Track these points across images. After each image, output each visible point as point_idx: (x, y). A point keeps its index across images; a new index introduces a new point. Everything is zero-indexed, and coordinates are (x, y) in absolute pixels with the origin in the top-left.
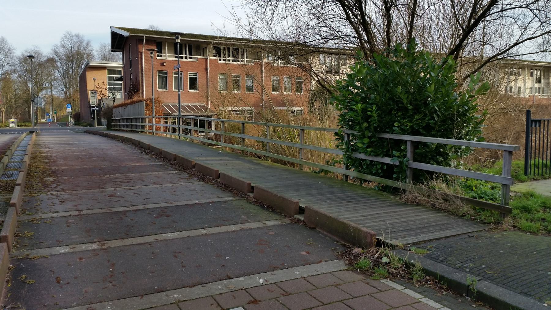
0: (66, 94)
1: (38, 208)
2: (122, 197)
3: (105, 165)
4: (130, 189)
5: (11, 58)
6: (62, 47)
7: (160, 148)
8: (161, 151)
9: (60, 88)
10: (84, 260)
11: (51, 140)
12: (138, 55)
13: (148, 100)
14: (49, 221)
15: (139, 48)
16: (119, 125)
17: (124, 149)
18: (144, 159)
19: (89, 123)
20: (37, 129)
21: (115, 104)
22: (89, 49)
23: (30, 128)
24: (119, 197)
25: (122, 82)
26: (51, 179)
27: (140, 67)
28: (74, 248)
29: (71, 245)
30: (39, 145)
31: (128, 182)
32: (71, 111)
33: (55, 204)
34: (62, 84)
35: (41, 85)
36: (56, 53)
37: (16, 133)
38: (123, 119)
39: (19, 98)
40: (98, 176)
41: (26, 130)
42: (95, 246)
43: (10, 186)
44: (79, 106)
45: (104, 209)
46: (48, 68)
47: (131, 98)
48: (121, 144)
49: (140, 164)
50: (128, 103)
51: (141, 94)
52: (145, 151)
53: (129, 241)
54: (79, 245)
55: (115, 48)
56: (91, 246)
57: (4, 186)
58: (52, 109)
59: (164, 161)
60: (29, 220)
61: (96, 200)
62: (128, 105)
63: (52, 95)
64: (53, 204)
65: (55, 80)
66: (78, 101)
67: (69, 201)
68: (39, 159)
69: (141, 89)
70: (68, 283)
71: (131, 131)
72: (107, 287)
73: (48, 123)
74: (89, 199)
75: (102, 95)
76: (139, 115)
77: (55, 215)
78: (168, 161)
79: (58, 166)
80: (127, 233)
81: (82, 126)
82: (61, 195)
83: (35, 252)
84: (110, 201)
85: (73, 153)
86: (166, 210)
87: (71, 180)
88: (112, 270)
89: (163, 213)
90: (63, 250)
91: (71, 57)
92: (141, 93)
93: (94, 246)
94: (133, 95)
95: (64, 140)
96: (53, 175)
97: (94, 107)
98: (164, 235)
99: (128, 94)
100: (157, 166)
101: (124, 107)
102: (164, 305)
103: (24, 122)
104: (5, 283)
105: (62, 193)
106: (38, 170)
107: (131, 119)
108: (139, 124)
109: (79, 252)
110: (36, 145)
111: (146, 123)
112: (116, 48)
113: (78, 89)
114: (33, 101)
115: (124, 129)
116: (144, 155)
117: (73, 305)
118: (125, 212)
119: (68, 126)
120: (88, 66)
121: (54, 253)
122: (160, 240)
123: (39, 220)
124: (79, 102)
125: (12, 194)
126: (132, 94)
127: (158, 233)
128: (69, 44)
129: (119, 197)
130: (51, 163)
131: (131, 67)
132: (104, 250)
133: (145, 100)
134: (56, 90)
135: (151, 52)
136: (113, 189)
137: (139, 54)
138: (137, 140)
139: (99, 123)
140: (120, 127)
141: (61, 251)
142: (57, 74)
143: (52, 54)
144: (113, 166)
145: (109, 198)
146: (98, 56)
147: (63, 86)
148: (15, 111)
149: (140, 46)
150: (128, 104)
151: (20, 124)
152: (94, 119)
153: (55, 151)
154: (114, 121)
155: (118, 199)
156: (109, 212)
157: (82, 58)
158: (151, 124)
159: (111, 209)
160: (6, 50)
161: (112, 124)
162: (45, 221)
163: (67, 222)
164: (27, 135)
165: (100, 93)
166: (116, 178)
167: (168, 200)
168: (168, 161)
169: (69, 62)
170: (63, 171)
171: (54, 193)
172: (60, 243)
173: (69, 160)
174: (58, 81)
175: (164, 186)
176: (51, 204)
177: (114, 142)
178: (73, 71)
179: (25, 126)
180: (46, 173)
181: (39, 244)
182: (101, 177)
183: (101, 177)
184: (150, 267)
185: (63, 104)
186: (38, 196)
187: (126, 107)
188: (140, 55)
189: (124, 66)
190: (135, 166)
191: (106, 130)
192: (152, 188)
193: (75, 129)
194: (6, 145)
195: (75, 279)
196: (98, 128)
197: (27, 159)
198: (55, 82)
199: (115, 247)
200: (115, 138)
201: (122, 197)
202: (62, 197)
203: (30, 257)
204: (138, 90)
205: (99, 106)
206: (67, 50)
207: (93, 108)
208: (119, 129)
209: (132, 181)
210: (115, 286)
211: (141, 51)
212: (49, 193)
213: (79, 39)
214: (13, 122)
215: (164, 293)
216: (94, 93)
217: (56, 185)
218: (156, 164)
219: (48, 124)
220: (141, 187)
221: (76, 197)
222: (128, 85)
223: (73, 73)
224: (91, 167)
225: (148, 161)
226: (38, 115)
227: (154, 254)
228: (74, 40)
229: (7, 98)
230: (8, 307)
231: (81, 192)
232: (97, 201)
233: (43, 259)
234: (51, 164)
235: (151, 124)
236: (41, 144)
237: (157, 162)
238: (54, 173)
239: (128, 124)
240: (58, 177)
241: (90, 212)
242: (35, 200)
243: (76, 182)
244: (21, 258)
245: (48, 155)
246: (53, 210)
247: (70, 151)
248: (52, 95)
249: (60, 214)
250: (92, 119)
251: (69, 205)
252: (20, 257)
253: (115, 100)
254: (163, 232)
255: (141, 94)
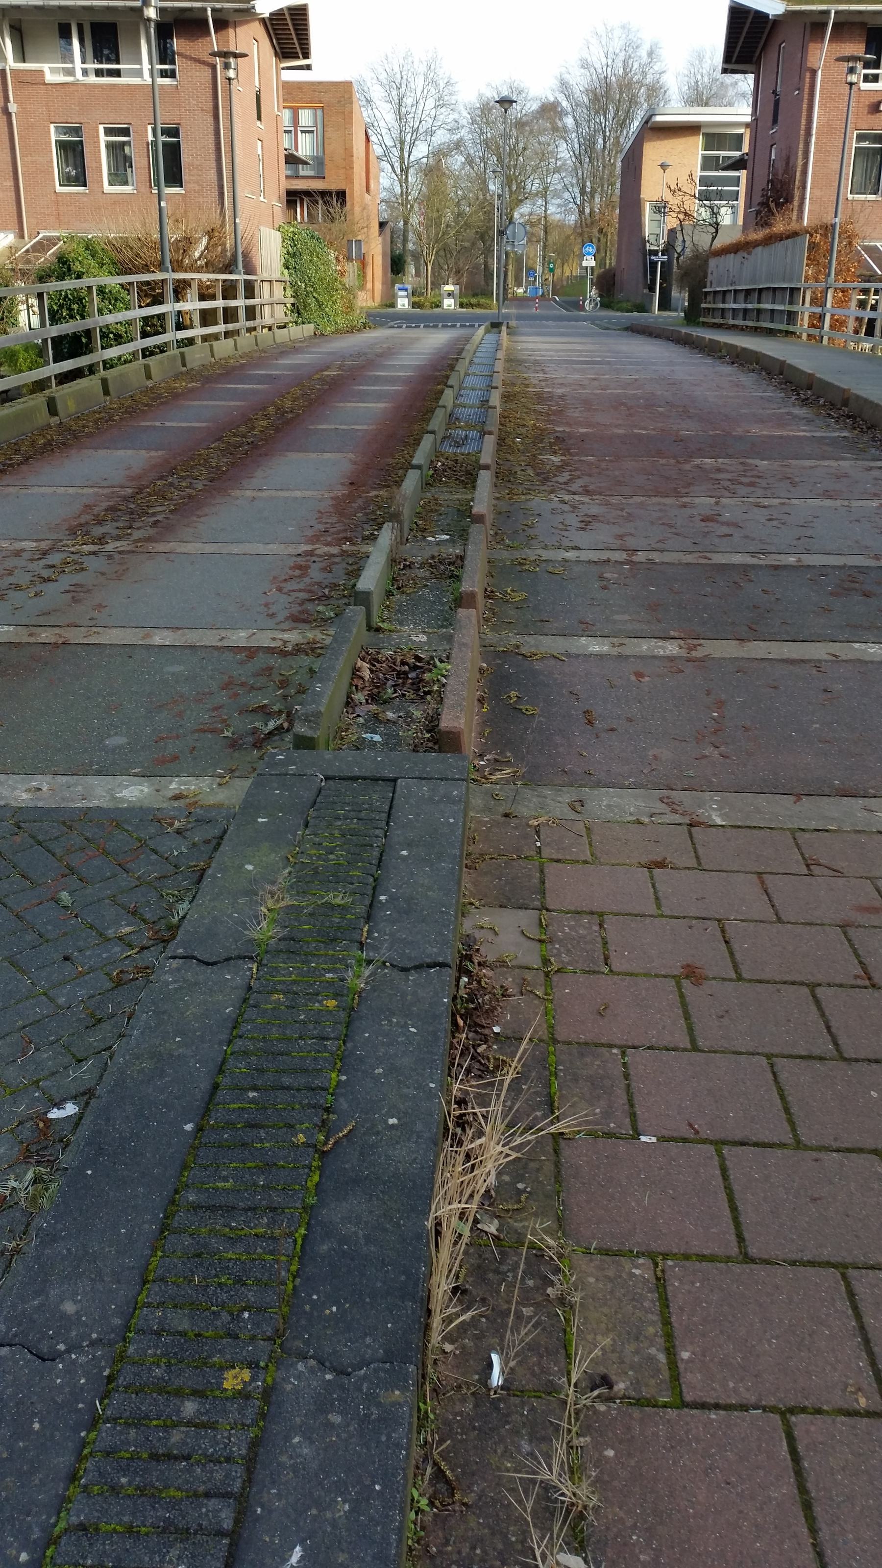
0: (581, 212)
1: (530, 532)
2: (737, 526)
3: (688, 429)
4: (757, 505)
5: (452, 107)
6: (582, 67)
7: (846, 387)
8: (846, 396)
9: (566, 195)
10: (647, 679)
11: (547, 350)
12: (801, 78)
13: (816, 232)
14: (559, 570)
15: (810, 53)
16: (723, 309)
17: (737, 386)
18: (795, 417)
19: (638, 302)
20: (508, 317)
21: (718, 244)
22: (657, 67)
23: (489, 311)
24: (727, 524)
25: (743, 174)
26: (556, 459)
27: (803, 122)
28: (621, 645)
29: (616, 637)
30: (520, 362)
31: (752, 484)
32: (593, 264)
33: (569, 528)
34: (574, 181)
35: (521, 187)
36: (564, 86)
37: (458, 324)
38: (735, 291)
39: (467, 225)
40: (672, 461)
41: (480, 319)
42: (672, 648)
43: (463, 469)
44: (614, 250)
45: (691, 552)
46: (541, 132)
47: (767, 224)
48: (727, 369)
49: (785, 433)
50: (756, 240)
51: (795, 213)
52: (798, 394)
53: (758, 649)
54: (632, 640)
55: (734, 60)
56: (663, 648)
57: (450, 468)
58: (544, 258)
59: (854, 428)
60: (512, 560)
61: (671, 526)
62: (754, 247)
63: (545, 217)
64: (566, 527)
65: (557, 170)
66: (612, 232)
67: (599, 521)
68: (524, 400)
69: (797, 193)
70: (612, 730)
71: (756, 328)
72: (706, 756)
73: (533, 299)
74: (652, 523)
75: (681, 217)
76: (784, 281)
77: (571, 555)
78: (868, 428)
79: (569, 425)
80: (753, 626)
81: (618, 310)
82: (583, 503)
83: (533, 642)
84: (706, 534)
85: (605, 390)
86: (861, 578)
87: (603, 465)
88: (719, 716)
89: (853, 585)
90: (597, 647)
91: (602, 96)
92: (796, 209)
93: (670, 647)
94: (773, 214)
95: (579, 351)
96: (560, 449)
97: (655, 253)
98: (857, 645)
99: (758, 212)
100: (834, 442)
101: (741, 254)
102: (859, 832)
103: (475, 295)
104: (476, 702)
105: (586, 499)
106: (523, 430)
107: (761, 290)
108: (782, 308)
109: (634, 656)
110: (513, 361)
111: (803, 304)
112: (737, 62)
113: (616, 199)
114: (501, 233)
115: (736, 322)
116: (794, 405)
117: (627, 783)
118: (745, 569)
119: (582, 308)
120: (649, 125)
121: (574, 651)
122: (844, 658)
123: (538, 562)
124: (616, 238)
125: (474, 487)
126: (770, 210)
127: (841, 638)
128: (602, 55)
129: (727, 524)
130: (554, 415)
131: (775, 121)
132: (696, 663)
133: (807, 232)
134: (558, 201)
135: (851, 65)
136: (713, 500)
137: (808, 75)
138: (776, 356)
139: (665, 304)
140: (723, 317)
141: (591, 649)
142: (564, 152)
143: (553, 90)
144: (711, 433)
145: (703, 524)
146: (680, 89)
147: (577, 190)
148: (456, 263)
149: (812, 46)
150: (756, 244)
151: (465, 300)
152: (652, 289)
153: (560, 381)
154: (710, 298)
155: (725, 530)
156: (706, 565)
157: (633, 101)
158: (818, 310)
159: (708, 555)
160: (442, 85)
161: (703, 306)
162: (550, 569)
163: (601, 578)
164: (487, 331)
165: (677, 210)
166: (719, 470)
167: (867, 547)
168: (868, 428)
169: (597, 112)
170: (583, 438)
171: (567, 498)
172: (587, 629)
173: (597, 409)
174: (563, 174)
175: (855, 504)
176: (561, 526)
177: (709, 360)
178: (605, 142)
179: (478, 305)
180: (541, 441)
181: (539, 624)
182: (678, 462)
183: (678, 462)
184: (818, 726)
185: (570, 244)
186: (529, 503)
187: (749, 253)
188: (808, 80)
189: (756, 120)
190: (770, 437)
191: (682, 325)
192: (821, 507)
193: (601, 319)
194: (443, 358)
195: (629, 724)
196: (659, 317)
197: (495, 399)
198: (557, 176)
199: (724, 659)
200: (712, 350)
201: (737, 526)
202: (584, 509)
203: (523, 651)
204: (789, 200)
205: (669, 249)
206: (594, 77)
207: (653, 257)
208: (722, 321)
209: (763, 482)
210: (727, 757)
211: (815, 67)
212: (552, 496)
213: (630, 37)
214: (450, 295)
215: (860, 801)
216: (661, 208)
217: (569, 477)
218: (829, 434)
219: (531, 303)
220: (787, 501)
221: (619, 513)
222: (761, 183)
223: (604, 146)
224: (653, 433)
225: (805, 425)
226: (510, 274)
227: (829, 695)
228: (616, 40)
229: (438, 225)
230: (488, 757)
231: (631, 501)
232: (674, 530)
233: (553, 662)
234: (552, 418)
235: (818, 310)
236: (525, 361)
237: (834, 430)
238: (560, 443)
239: (749, 306)
240: (571, 454)
241: (656, 557)
242: (521, 511)
243: (617, 473)
244: (504, 651)
245: (543, 393)
246: (566, 543)
247: (596, 383)
248: (545, 217)
249: (585, 555)
250: (646, 291)
251: (603, 534)
252: (501, 649)
253: (717, 231)
254: (855, 639)
255: (795, 213)
